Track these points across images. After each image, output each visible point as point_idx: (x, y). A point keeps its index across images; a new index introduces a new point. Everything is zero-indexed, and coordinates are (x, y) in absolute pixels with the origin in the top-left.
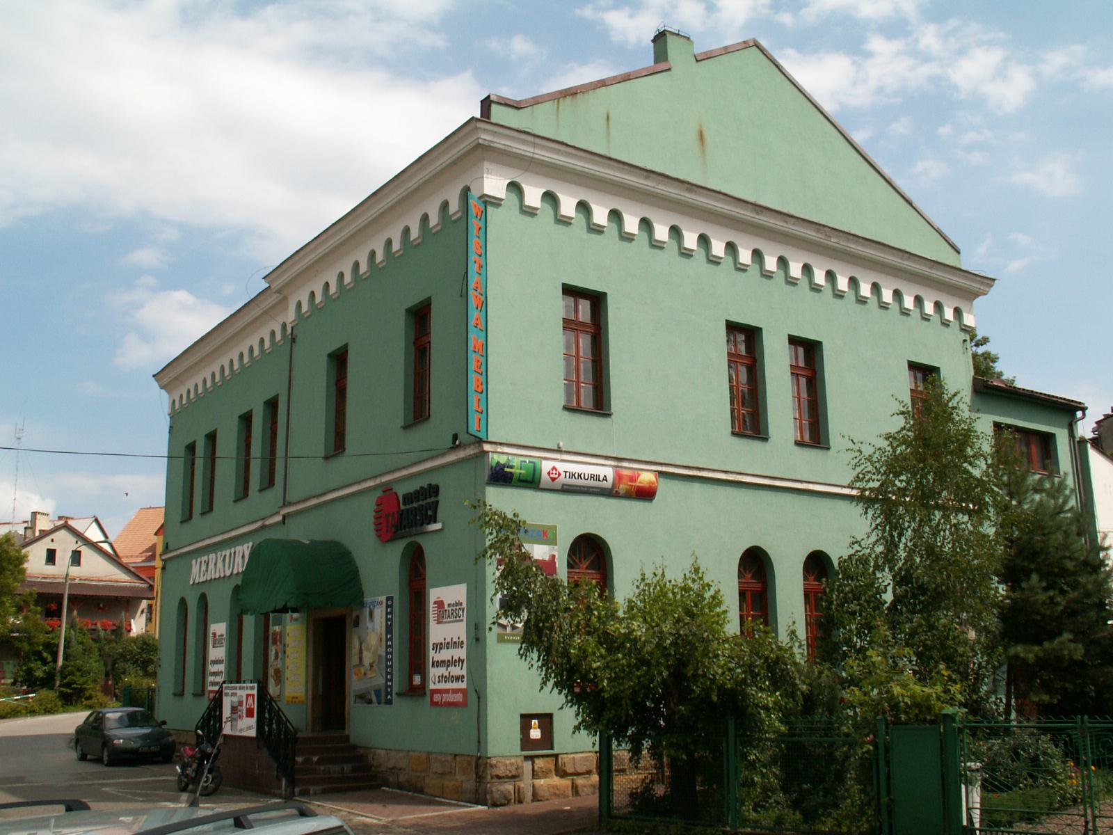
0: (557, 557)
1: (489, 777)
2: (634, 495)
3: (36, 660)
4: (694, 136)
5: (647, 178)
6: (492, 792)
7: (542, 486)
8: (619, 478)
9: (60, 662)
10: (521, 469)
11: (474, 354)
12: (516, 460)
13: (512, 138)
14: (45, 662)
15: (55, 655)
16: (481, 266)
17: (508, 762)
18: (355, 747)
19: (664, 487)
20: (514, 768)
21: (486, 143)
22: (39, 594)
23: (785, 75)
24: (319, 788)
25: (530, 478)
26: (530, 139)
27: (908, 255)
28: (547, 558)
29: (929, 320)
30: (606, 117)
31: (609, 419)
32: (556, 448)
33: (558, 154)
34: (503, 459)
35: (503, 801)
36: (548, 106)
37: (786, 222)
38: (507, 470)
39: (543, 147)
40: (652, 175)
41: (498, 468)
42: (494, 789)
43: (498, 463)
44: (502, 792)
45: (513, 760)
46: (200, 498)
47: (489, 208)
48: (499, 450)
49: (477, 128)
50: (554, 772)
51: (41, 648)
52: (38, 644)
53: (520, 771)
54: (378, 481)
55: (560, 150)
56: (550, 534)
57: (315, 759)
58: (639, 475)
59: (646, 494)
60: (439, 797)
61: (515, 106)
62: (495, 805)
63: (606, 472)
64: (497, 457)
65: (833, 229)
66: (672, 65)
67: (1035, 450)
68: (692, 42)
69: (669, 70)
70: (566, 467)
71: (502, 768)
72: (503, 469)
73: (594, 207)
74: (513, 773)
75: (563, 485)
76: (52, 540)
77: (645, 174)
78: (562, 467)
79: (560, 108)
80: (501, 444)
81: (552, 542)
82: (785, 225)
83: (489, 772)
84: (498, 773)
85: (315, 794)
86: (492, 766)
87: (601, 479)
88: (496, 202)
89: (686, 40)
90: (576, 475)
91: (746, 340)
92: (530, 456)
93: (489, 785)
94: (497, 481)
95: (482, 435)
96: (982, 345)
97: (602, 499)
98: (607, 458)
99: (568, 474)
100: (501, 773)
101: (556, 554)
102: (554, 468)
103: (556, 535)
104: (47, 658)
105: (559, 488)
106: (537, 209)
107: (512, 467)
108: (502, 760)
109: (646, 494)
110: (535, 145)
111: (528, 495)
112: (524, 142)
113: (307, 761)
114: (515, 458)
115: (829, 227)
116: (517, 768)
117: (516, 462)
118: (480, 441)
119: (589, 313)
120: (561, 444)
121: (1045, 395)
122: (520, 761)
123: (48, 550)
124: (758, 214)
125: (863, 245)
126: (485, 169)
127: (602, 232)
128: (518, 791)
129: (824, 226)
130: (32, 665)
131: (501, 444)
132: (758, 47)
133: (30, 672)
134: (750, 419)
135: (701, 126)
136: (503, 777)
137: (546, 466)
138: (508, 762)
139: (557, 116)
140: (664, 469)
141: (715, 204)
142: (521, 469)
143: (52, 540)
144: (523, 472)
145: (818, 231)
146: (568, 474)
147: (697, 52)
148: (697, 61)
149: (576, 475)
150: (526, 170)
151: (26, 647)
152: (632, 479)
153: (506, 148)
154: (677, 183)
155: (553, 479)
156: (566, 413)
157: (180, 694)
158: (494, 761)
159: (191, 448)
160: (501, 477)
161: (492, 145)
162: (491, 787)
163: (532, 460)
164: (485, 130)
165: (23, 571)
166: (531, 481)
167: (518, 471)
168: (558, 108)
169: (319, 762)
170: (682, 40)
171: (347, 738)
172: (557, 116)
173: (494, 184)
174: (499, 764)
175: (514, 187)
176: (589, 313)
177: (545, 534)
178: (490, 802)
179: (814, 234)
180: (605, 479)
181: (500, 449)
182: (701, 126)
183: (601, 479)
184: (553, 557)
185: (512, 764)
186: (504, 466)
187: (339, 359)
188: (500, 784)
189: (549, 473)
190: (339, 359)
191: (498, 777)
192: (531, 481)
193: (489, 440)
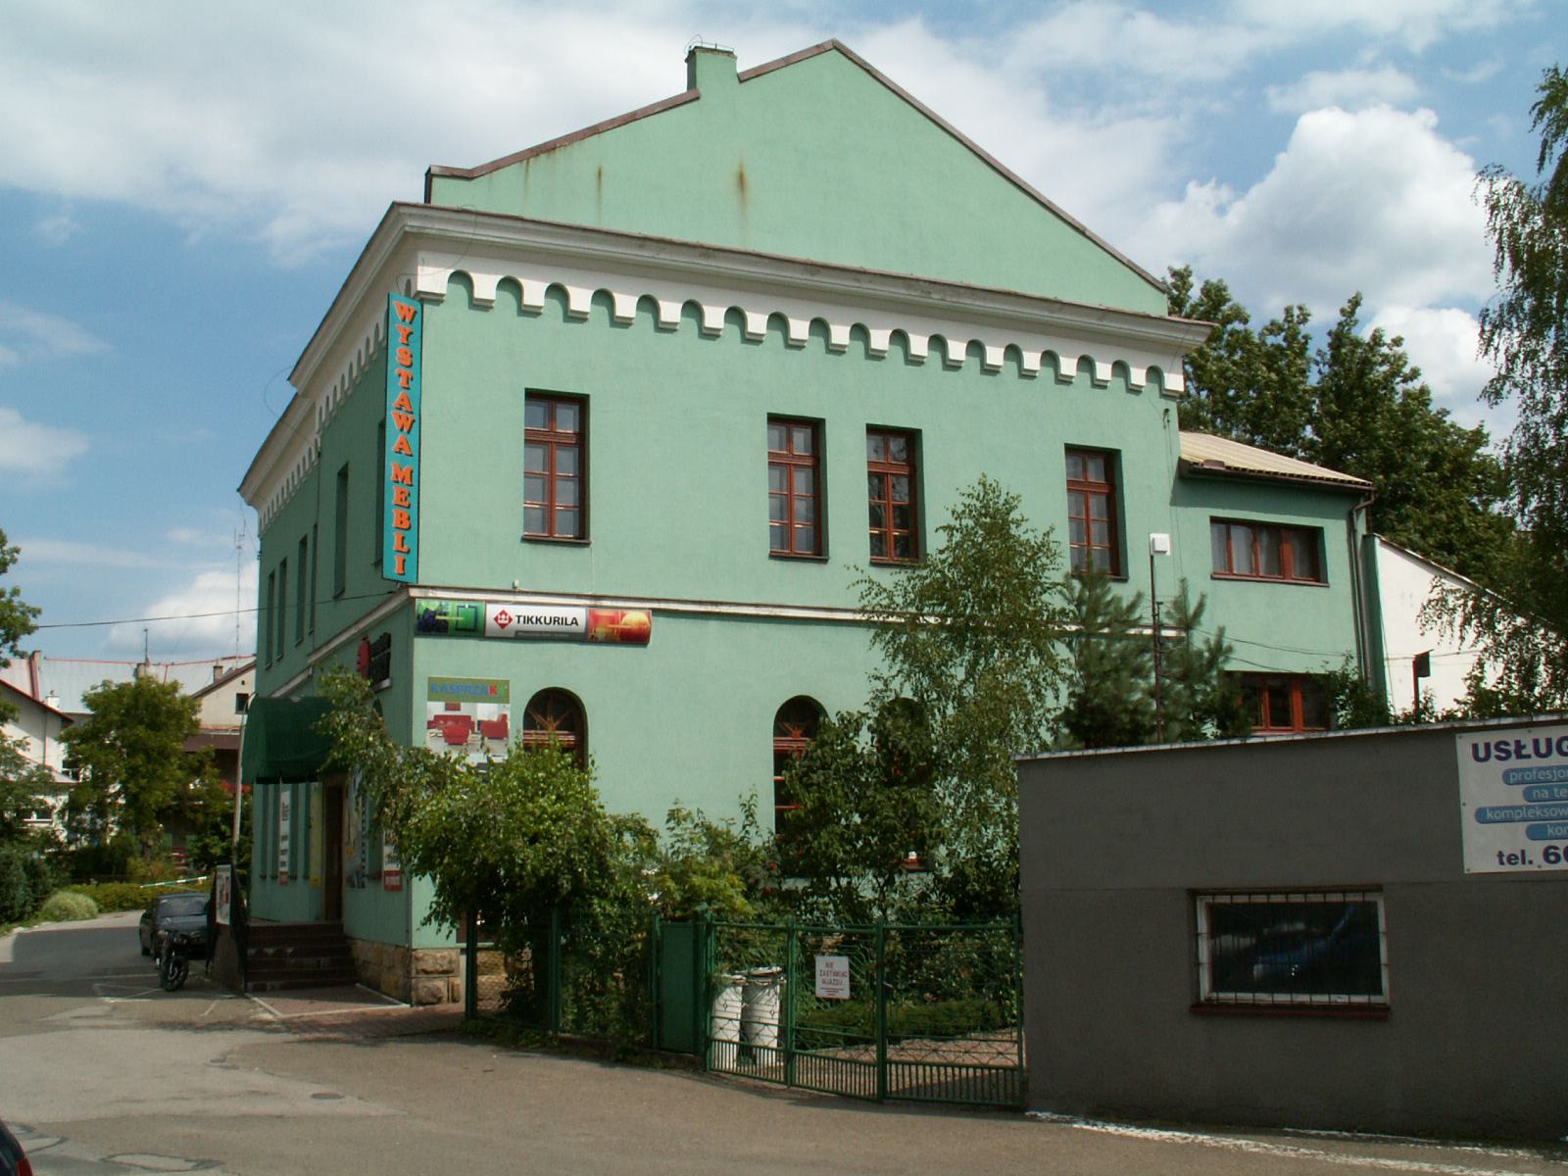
0: (509, 717)
1: (414, 971)
2: (619, 639)
3: (213, 835)
4: (731, 181)
5: (641, 247)
6: (417, 989)
7: (488, 634)
8: (593, 619)
9: (237, 837)
10: (458, 615)
11: (395, 486)
12: (451, 604)
13: (449, 221)
14: (223, 837)
15: (232, 826)
16: (409, 379)
17: (438, 955)
18: (346, 937)
19: (660, 628)
20: (446, 962)
21: (415, 230)
22: (217, 751)
23: (882, 82)
24: (276, 983)
25: (472, 627)
26: (472, 218)
27: (1058, 305)
28: (495, 719)
29: (1105, 387)
30: (596, 173)
31: (586, 549)
32: (510, 588)
33: (514, 232)
34: (433, 606)
35: (431, 1000)
36: (515, 169)
37: (858, 281)
38: (438, 617)
39: (484, 226)
40: (648, 243)
41: (427, 617)
42: (420, 985)
43: (427, 610)
44: (429, 989)
45: (445, 953)
46: (1311, 519)
47: (427, 307)
48: (430, 595)
49: (400, 214)
50: (502, 968)
51: (219, 819)
52: (215, 815)
53: (454, 966)
54: (353, 631)
55: (514, 228)
56: (501, 691)
57: (290, 950)
58: (623, 615)
59: (637, 638)
60: (388, 995)
61: (466, 176)
62: (420, 1003)
63: (577, 614)
64: (426, 604)
65: (931, 282)
66: (701, 91)
67: (1292, 551)
68: (735, 58)
69: (698, 98)
70: (518, 611)
71: (430, 962)
72: (434, 617)
73: (571, 290)
74: (445, 968)
75: (517, 632)
76: (243, 683)
77: (639, 242)
78: (513, 611)
79: (530, 170)
80: (433, 588)
81: (504, 699)
82: (857, 285)
83: (413, 966)
84: (425, 967)
85: (273, 989)
86: (417, 959)
87: (569, 622)
88: (436, 299)
89: (725, 57)
90: (534, 620)
91: (800, 440)
92: (469, 600)
93: (413, 981)
94: (429, 631)
95: (409, 578)
96: (1412, 380)
97: (575, 647)
98: (579, 596)
99: (522, 619)
100: (429, 966)
101: (508, 713)
102: (503, 613)
103: (508, 690)
104: (225, 832)
105: (513, 635)
106: (492, 301)
107: (445, 614)
108: (427, 952)
109: (637, 638)
110: (476, 224)
111: (470, 645)
112: (465, 223)
113: (260, 953)
114: (451, 603)
115: (925, 281)
116: (450, 962)
117: (451, 607)
118: (406, 586)
119: (560, 421)
120: (517, 584)
121: (1299, 476)
122: (454, 954)
123: (238, 695)
124: (812, 275)
125: (984, 299)
126: (420, 260)
127: (585, 320)
128: (452, 988)
129: (917, 280)
130: (207, 840)
131: (433, 588)
132: (838, 50)
133: (205, 848)
134: (803, 538)
135: (741, 166)
136: (432, 972)
137: (492, 611)
138: (438, 955)
139: (526, 179)
140: (656, 605)
141: (746, 268)
142: (458, 615)
143: (243, 683)
144: (460, 618)
145: (909, 287)
146: (522, 619)
147: (740, 70)
148: (741, 82)
149: (534, 620)
150: (465, 254)
151: (201, 818)
152: (613, 620)
153: (443, 233)
154: (685, 249)
155: (503, 626)
156: (527, 546)
157: (264, 877)
158: (420, 954)
159: (272, 577)
160: (433, 626)
161: (422, 231)
162: (417, 983)
163: (473, 604)
164: (411, 215)
165: (196, 724)
166: (473, 629)
167: (454, 618)
168: (527, 170)
169: (293, 955)
170: (721, 57)
171: (341, 927)
172: (526, 179)
173: (431, 277)
174: (426, 958)
175: (461, 278)
176: (560, 421)
177: (493, 690)
178: (414, 999)
179: (904, 291)
180: (575, 622)
181: (431, 594)
182: (741, 166)
183: (569, 622)
184: (504, 717)
185: (443, 957)
186: (435, 613)
187: (343, 475)
188: (429, 979)
189: (496, 619)
190: (343, 475)
191: (425, 972)
192: (473, 629)
193: (420, 583)
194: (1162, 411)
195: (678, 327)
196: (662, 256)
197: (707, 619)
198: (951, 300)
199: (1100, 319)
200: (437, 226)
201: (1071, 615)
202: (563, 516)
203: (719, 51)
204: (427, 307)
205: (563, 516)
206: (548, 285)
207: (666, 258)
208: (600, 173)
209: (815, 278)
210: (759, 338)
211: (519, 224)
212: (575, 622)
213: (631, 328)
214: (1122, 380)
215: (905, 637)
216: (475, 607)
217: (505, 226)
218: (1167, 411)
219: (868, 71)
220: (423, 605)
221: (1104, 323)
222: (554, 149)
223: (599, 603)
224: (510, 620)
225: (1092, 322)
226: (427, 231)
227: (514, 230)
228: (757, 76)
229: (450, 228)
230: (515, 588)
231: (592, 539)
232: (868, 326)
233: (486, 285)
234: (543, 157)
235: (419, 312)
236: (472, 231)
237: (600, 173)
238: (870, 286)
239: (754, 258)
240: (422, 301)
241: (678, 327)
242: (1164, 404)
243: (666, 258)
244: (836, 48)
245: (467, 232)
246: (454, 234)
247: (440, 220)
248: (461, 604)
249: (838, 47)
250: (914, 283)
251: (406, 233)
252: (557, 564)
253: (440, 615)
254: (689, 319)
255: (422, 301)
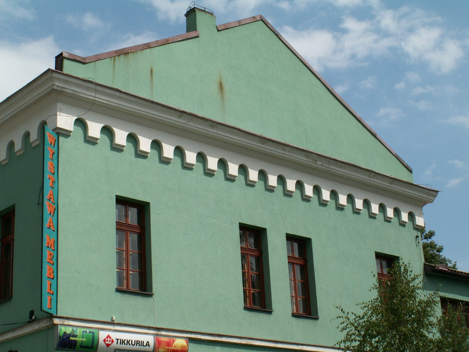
5: (180, 117)
21: (59, 89)
25: (90, 346)
26: (93, 86)
27: (373, 174)
32: (110, 321)
34: (69, 330)
37: (284, 150)
40: (184, 115)
43: (65, 333)
47: (61, 139)
48: (66, 323)
58: (174, 341)
69: (198, 37)
77: (179, 114)
78: (114, 336)
80: (67, 318)
82: (283, 152)
87: (145, 344)
88: (66, 134)
89: (210, 15)
90: (126, 342)
91: (253, 237)
92: (90, 328)
94: (65, 347)
95: (53, 312)
98: (149, 328)
99: (119, 341)
102: (109, 336)
107: (76, 336)
110: (96, 91)
112: (88, 89)
115: (315, 154)
117: (79, 332)
118: (51, 316)
120: (114, 318)
124: (263, 144)
125: (341, 167)
126: (58, 109)
129: (312, 153)
131: (67, 318)
135: (221, 78)
137: (102, 335)
140: (193, 336)
144: (84, 340)
145: (307, 157)
146: (119, 341)
148: (218, 31)
149: (126, 342)
152: (169, 344)
155: (108, 345)
163: (92, 330)
167: (81, 339)
173: (65, 120)
175: (80, 123)
180: (148, 344)
181: (66, 322)
182: (221, 78)
183: (145, 344)
189: (104, 341)
193: (59, 315)
194: (415, 237)
195: (98, 142)
196: (190, 123)
197: (215, 345)
198: (326, 166)
199: (391, 183)
200: (72, 88)
201: (428, 307)
202: (138, 277)
203: (207, 12)
204: (61, 139)
205: (138, 277)
206: (128, 133)
207: (192, 125)
208: (152, 71)
209: (264, 146)
210: (121, 148)
211: (118, 94)
212: (148, 344)
213: (69, 138)
214: (263, 182)
215: (381, 314)
216: (93, 332)
217: (109, 94)
218: (417, 237)
219: (277, 35)
220: (63, 330)
221: (392, 186)
222: (128, 53)
223: (160, 333)
224: (113, 341)
225: (386, 184)
226: (66, 90)
227: (113, 96)
228: (226, 29)
229: (67, 87)
230: (113, 321)
231: (154, 291)
232: (354, 196)
233: (95, 129)
234: (122, 57)
235: (57, 140)
236: (94, 95)
237: (152, 71)
238: (289, 154)
239: (236, 131)
240: (58, 134)
241: (98, 142)
242: (416, 233)
243: (192, 125)
244: (262, 20)
245: (90, 95)
246: (81, 95)
247: (76, 85)
248: (85, 330)
249: (263, 20)
250: (310, 154)
251: (54, 89)
252: (133, 306)
253: (73, 336)
254: (177, 157)
255: (58, 134)
